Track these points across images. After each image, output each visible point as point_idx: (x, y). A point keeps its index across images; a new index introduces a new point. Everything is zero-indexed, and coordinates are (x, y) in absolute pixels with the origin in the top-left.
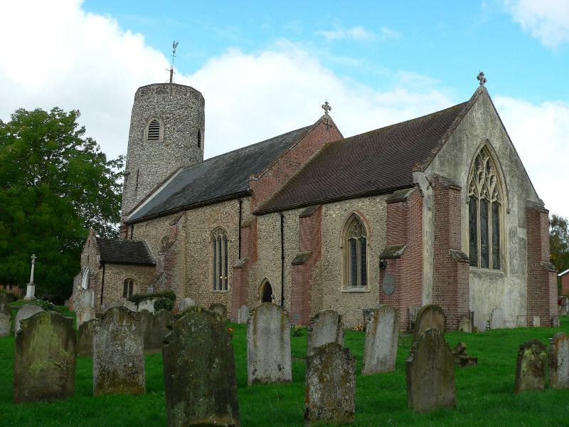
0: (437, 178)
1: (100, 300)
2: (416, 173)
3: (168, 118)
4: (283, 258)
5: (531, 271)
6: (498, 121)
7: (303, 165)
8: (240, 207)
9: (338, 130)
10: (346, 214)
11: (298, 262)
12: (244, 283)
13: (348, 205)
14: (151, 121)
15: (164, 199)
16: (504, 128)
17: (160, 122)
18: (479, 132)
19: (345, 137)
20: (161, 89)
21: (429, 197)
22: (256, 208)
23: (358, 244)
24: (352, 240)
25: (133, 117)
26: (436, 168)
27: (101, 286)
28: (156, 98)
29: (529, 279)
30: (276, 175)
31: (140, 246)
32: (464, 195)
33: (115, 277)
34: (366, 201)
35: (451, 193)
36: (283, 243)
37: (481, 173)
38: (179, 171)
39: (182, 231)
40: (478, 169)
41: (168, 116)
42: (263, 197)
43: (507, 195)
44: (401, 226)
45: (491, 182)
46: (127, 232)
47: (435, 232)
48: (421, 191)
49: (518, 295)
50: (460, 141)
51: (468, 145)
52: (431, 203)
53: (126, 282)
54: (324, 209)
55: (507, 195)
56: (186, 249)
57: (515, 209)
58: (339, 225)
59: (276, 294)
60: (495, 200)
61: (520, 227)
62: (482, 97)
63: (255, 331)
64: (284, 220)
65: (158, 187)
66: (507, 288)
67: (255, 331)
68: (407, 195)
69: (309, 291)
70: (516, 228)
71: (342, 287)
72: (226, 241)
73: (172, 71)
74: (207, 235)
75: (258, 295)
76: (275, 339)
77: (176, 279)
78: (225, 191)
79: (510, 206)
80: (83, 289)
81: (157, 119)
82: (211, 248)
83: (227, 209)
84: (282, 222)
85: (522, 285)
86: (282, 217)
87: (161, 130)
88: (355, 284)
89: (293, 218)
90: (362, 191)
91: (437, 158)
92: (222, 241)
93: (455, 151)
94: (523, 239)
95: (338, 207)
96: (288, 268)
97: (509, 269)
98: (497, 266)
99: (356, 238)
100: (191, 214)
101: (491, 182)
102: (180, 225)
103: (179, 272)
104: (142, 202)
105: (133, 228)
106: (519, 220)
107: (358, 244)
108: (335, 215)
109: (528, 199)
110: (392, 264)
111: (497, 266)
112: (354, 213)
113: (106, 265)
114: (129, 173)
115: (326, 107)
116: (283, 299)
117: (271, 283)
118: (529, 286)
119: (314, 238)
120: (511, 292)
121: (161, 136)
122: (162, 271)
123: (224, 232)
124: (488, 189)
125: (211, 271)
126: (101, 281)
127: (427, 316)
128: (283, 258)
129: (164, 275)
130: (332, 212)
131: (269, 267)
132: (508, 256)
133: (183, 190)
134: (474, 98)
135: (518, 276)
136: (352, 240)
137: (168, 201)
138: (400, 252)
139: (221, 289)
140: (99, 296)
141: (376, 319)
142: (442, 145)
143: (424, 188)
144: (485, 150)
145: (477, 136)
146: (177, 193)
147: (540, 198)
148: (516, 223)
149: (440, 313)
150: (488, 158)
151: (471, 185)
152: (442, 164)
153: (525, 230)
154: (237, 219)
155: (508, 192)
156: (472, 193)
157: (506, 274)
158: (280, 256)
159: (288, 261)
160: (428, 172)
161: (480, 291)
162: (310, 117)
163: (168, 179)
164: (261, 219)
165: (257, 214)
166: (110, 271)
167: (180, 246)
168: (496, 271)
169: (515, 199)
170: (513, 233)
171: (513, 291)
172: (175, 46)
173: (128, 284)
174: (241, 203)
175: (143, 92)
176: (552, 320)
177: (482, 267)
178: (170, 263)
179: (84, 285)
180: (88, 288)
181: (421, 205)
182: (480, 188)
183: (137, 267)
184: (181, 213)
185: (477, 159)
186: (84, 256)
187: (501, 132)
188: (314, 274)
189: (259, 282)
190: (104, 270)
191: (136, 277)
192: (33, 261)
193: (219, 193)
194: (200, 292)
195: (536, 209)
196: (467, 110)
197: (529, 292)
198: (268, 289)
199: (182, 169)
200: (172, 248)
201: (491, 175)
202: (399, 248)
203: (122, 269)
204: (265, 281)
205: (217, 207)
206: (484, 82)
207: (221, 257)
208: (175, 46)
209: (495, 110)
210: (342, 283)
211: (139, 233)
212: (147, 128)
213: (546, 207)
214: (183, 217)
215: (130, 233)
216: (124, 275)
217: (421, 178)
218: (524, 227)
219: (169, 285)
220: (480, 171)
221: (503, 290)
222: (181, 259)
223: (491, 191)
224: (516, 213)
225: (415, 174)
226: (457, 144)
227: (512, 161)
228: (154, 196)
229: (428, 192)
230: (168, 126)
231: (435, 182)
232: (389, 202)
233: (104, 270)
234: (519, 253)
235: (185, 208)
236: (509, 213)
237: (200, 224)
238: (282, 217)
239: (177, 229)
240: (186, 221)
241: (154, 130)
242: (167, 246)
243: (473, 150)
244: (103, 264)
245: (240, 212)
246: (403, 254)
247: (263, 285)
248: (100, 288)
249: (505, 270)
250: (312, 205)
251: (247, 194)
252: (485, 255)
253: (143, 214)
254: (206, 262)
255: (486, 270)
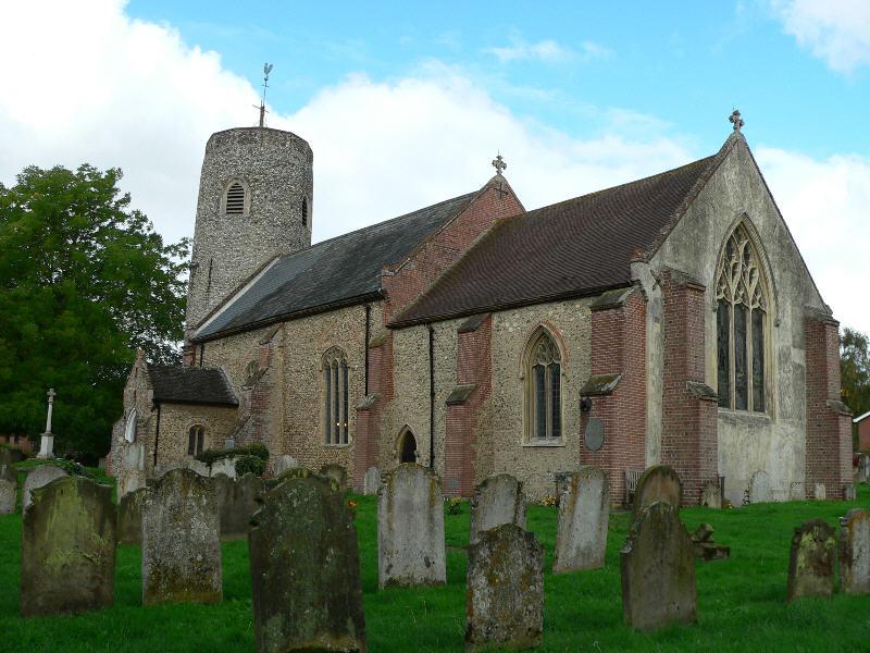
0: (668, 272)
1: (153, 459)
2: (637, 264)
3: (257, 180)
4: (433, 394)
5: (812, 415)
6: (761, 185)
7: (463, 253)
8: (368, 316)
9: (516, 199)
10: (530, 328)
11: (456, 401)
12: (373, 432)
13: (532, 313)
14: (231, 184)
15: (251, 305)
16: (771, 196)
17: (245, 186)
18: (732, 201)
19: (528, 209)
20: (246, 136)
21: (656, 301)
22: (391, 319)
23: (548, 373)
24: (538, 367)
25: (203, 179)
26: (667, 256)
27: (154, 438)
28: (238, 150)
29: (809, 427)
30: (422, 267)
31: (215, 377)
32: (710, 298)
33: (176, 424)
34: (560, 307)
35: (690, 295)
36: (432, 372)
37: (735, 265)
38: (274, 262)
39: (279, 354)
40: (730, 258)
41: (257, 177)
42: (401, 306)
43: (776, 298)
44: (613, 346)
45: (751, 278)
46: (193, 355)
47: (665, 355)
48: (644, 291)
49: (791, 451)
50: (704, 216)
51: (715, 222)
52: (659, 311)
53: (192, 431)
54: (495, 319)
55: (776, 298)
56: (285, 380)
57: (787, 320)
58: (519, 344)
59: (422, 449)
60: (757, 305)
61: (795, 347)
62: (736, 149)
63: (390, 507)
64: (435, 337)
65: (242, 287)
66: (775, 440)
67: (390, 507)
68: (622, 298)
69: (472, 445)
70: (788, 348)
71: (522, 440)
72: (346, 369)
73: (263, 109)
74: (317, 360)
75: (394, 452)
76: (421, 519)
77: (269, 426)
78: (343, 292)
79: (780, 314)
80: (127, 442)
81: (239, 182)
82: (322, 380)
83: (347, 320)
84: (432, 339)
85: (799, 436)
86: (432, 331)
87: (247, 199)
88: (542, 434)
89: (447, 333)
90: (554, 292)
91: (668, 242)
92: (340, 369)
93: (696, 231)
94: (800, 366)
95: (517, 316)
96: (441, 410)
97: (778, 411)
98: (760, 407)
99: (545, 364)
100: (292, 328)
101: (751, 278)
102: (275, 343)
103: (273, 415)
104: (218, 308)
105: (203, 349)
106: (794, 337)
107: (548, 373)
108: (512, 328)
109: (807, 305)
110: (599, 404)
111: (760, 407)
112: (541, 326)
113: (162, 406)
114: (198, 265)
115: (499, 164)
116: (432, 457)
117: (414, 432)
118: (808, 437)
119: (481, 364)
120: (781, 446)
121: (247, 207)
122: (248, 414)
123: (343, 354)
124: (746, 290)
125: (322, 414)
126: (154, 429)
127: (653, 483)
128: (433, 394)
129: (252, 421)
130: (507, 325)
131: (411, 409)
132: (776, 392)
133: (281, 290)
134: (725, 150)
135: (793, 422)
136: (538, 367)
137: (257, 308)
138: (612, 385)
139: (338, 442)
140: (152, 453)
141: (575, 487)
142: (676, 222)
143: (648, 288)
144: (742, 229)
145: (730, 208)
146: (271, 296)
147: (826, 302)
148: (789, 341)
149: (673, 478)
150: (745, 242)
151: (721, 283)
152: (676, 250)
153: (803, 352)
154: (362, 335)
155: (776, 293)
156: (722, 296)
157: (773, 419)
158: (427, 391)
159: (441, 399)
160: (655, 263)
161: (734, 446)
162: (474, 179)
163: (257, 274)
164: (399, 336)
165: (393, 327)
166: (168, 415)
167: (275, 376)
168: (758, 415)
169: (788, 304)
170: (784, 357)
171: (784, 445)
172: (267, 70)
173: (196, 434)
174: (368, 310)
175: (219, 141)
176: (844, 489)
177: (737, 408)
178: (260, 402)
179: (129, 436)
180: (135, 440)
181: (644, 314)
182: (733, 288)
183: (209, 409)
184: (277, 326)
185: (729, 243)
186: (128, 391)
187: (766, 202)
188: (480, 420)
189: (396, 431)
190: (159, 412)
191: (208, 424)
192: (51, 399)
193: (334, 296)
194: (307, 447)
195: (819, 319)
196: (715, 168)
197: (809, 447)
198: (409, 442)
199: (278, 259)
200: (264, 379)
201: (750, 267)
202: (610, 380)
203: (186, 411)
204: (406, 430)
205: (332, 317)
206: (741, 125)
207: (337, 394)
208: (267, 70)
209: (757, 168)
210: (523, 433)
211: (213, 356)
212: (225, 195)
213: (835, 317)
214: (280, 331)
215: (198, 357)
216: (190, 421)
217: (643, 272)
218: (801, 348)
219: (258, 436)
220: (734, 261)
221: (769, 443)
222: (276, 396)
223: (751, 292)
224: (789, 326)
225: (634, 267)
226: (699, 220)
227: (782, 247)
228: (235, 299)
229: (654, 294)
230: (257, 192)
231: (665, 279)
232: (594, 309)
233: (159, 412)
234: (794, 387)
235: (283, 319)
236: (778, 326)
237: (306, 343)
238: (432, 331)
239: (271, 350)
240: (284, 339)
241: (235, 198)
242: (256, 376)
243: (723, 229)
244: (157, 403)
245: (367, 324)
246: (616, 388)
247: (402, 436)
248: (153, 441)
249: (772, 413)
250: (477, 314)
251: (378, 297)
252: (742, 391)
253: (218, 327)
254: (315, 401)
255: (743, 413)
